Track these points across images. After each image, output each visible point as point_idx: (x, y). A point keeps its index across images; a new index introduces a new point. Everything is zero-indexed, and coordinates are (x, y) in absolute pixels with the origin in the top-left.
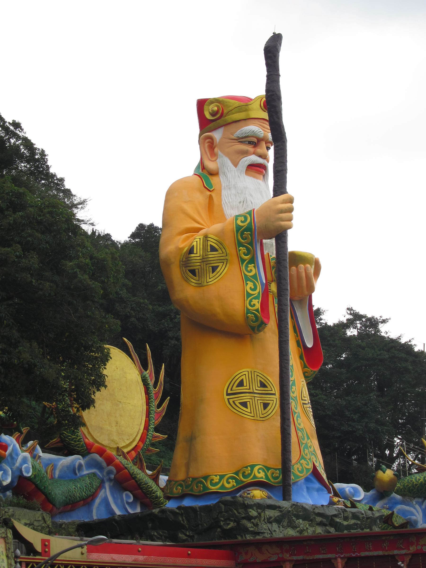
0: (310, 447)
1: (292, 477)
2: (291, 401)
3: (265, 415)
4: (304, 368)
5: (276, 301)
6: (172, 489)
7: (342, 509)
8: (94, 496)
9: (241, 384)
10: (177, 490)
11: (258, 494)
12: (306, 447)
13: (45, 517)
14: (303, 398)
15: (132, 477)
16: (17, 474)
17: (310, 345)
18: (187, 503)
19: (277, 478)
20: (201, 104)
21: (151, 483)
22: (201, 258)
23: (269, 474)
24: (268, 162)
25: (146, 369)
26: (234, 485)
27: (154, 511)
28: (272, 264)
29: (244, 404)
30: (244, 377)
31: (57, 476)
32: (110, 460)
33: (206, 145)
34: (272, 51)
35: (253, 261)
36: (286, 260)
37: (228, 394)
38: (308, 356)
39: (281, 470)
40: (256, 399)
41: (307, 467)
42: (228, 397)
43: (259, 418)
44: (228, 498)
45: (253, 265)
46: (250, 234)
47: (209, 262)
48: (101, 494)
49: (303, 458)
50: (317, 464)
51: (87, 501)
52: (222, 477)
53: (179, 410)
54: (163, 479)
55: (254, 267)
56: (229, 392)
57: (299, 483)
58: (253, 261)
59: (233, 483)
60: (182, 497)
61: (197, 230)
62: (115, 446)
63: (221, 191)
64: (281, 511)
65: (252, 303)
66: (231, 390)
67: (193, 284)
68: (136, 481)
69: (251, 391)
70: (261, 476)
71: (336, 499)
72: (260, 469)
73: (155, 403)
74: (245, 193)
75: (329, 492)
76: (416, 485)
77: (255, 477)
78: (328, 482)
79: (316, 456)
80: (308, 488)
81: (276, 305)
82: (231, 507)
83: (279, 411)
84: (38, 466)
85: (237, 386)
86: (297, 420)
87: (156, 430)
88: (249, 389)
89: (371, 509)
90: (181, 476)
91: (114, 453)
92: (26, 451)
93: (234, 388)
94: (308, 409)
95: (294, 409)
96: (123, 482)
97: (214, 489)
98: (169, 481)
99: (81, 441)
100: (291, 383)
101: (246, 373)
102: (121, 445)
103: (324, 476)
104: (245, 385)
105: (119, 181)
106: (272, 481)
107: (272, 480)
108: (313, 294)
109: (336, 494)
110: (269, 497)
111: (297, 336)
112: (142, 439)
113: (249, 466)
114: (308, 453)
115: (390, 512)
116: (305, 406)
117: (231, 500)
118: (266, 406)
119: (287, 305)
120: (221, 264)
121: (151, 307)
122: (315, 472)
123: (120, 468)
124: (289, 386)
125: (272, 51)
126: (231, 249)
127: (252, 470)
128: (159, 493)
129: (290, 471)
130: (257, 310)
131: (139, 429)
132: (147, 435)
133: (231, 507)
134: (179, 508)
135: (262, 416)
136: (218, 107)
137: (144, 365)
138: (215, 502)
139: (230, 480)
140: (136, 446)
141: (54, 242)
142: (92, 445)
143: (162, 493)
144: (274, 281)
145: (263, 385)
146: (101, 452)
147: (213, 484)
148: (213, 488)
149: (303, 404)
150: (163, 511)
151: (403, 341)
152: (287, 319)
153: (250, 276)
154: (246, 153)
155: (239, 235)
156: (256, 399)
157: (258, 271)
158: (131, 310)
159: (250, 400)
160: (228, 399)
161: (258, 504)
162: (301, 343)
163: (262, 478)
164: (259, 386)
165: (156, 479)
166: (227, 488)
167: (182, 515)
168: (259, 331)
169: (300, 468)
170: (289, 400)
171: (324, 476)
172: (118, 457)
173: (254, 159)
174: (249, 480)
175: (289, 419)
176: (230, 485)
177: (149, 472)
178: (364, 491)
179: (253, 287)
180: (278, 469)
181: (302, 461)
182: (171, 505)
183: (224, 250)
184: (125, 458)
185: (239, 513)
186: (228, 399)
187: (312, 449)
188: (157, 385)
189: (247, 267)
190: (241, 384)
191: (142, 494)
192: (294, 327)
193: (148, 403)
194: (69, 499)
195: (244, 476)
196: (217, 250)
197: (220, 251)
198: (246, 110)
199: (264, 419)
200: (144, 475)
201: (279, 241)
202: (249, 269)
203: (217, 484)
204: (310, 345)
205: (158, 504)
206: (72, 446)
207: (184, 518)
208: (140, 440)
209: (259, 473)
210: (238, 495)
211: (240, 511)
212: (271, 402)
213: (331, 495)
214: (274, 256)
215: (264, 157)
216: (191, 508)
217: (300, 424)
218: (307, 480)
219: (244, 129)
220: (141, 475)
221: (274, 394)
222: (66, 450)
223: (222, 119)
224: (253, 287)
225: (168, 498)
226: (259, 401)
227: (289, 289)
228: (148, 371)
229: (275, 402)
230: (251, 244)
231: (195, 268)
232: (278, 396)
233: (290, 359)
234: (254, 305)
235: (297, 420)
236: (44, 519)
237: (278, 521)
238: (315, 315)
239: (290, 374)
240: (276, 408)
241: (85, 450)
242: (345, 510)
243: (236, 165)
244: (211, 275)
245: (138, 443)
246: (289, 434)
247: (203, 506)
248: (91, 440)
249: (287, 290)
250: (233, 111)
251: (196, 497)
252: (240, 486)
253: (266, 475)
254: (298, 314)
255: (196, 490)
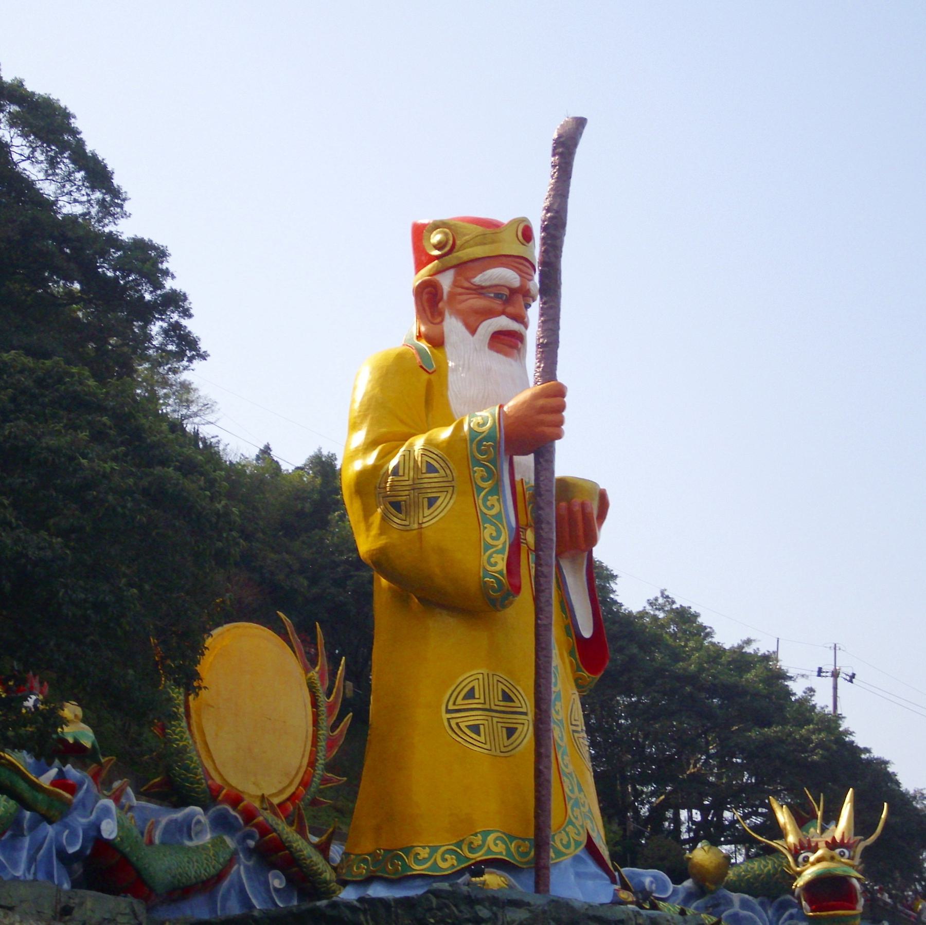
0: (584, 806)
1: (552, 854)
2: (553, 725)
3: (510, 748)
4: (578, 671)
5: (532, 557)
6: (350, 867)
7: (633, 911)
8: (220, 876)
9: (470, 694)
10: (362, 870)
11: (493, 880)
12: (577, 804)
13: (136, 909)
14: (574, 723)
15: (280, 845)
16: (93, 833)
17: (587, 633)
18: (377, 891)
19: (526, 854)
20: (419, 233)
21: (317, 858)
22: (410, 482)
23: (513, 847)
24: (526, 326)
25: (314, 663)
26: (453, 865)
27: (318, 903)
28: (527, 496)
29: (475, 729)
30: (475, 683)
31: (157, 840)
32: (249, 815)
33: (425, 297)
34: (565, 147)
35: (496, 489)
36: (551, 491)
37: (448, 711)
39: (533, 843)
40: (495, 720)
41: (576, 837)
42: (449, 716)
43: (498, 753)
44: (445, 886)
45: (496, 497)
46: (493, 447)
47: (423, 491)
49: (571, 823)
50: (594, 835)
52: (434, 849)
53: (367, 735)
54: (336, 851)
55: (498, 500)
56: (451, 707)
57: (562, 866)
58: (496, 489)
59: (452, 860)
60: (369, 880)
62: (260, 793)
63: (446, 376)
64: (530, 911)
65: (492, 560)
66: (454, 704)
67: (395, 526)
68: (291, 852)
69: (487, 706)
70: (498, 849)
71: (624, 895)
72: (497, 839)
73: (325, 722)
74: (483, 391)
75: (614, 881)
76: (759, 875)
77: (489, 851)
78: (613, 865)
79: (592, 820)
80: (578, 875)
81: (533, 565)
82: (446, 901)
83: (533, 743)
84: (127, 824)
85: (465, 698)
86: (563, 759)
87: (329, 767)
88: (485, 703)
89: (683, 913)
90: (367, 845)
91: (257, 804)
92: (109, 797)
93: (459, 701)
94: (581, 740)
95: (569, 793)
96: (271, 853)
97: (418, 869)
98: (346, 854)
99: (202, 784)
100: (553, 697)
101: (480, 676)
102: (267, 793)
103: (605, 852)
104: (477, 696)
105: (281, 369)
106: (516, 860)
107: (517, 857)
108: (594, 549)
109: (625, 887)
110: (511, 887)
111: (567, 618)
112: (305, 784)
113: (479, 833)
114: (580, 811)
115: (715, 919)
116: (576, 735)
117: (450, 889)
118: (511, 732)
119: (552, 549)
120: (443, 495)
122: (591, 847)
123: (265, 830)
124: (550, 700)
125: (565, 147)
127: (484, 841)
128: (329, 875)
129: (548, 844)
130: (500, 573)
131: (300, 767)
132: (314, 776)
133: (446, 901)
134: (361, 900)
135: (503, 749)
136: (446, 234)
137: (310, 661)
138: (420, 892)
139: (447, 856)
140: (294, 794)
142: (221, 788)
143: (334, 875)
144: (531, 526)
145: (507, 697)
146: (235, 800)
147: (418, 861)
148: (417, 867)
149: (574, 731)
150: (335, 905)
151: (891, 769)
152: (550, 589)
153: (492, 516)
154: (489, 313)
155: (474, 446)
156: (495, 720)
157: (503, 507)
159: (485, 722)
160: (448, 719)
161: (494, 897)
163: (501, 853)
164: (501, 698)
165: (323, 849)
166: (442, 869)
167: (365, 912)
168: (504, 607)
169: (565, 842)
170: (549, 725)
171: (605, 852)
172: (261, 811)
173: (504, 322)
174: (479, 856)
175: (549, 756)
176: (447, 865)
177: (315, 840)
178: (673, 883)
179: (494, 534)
180: (528, 840)
181: (570, 828)
182: (348, 894)
183: (448, 472)
184: (275, 814)
185: (461, 912)
186: (448, 719)
187: (586, 809)
188: (337, 727)
189: (485, 499)
190: (470, 694)
191: (302, 880)
192: (558, 582)
193: (316, 723)
194: (179, 880)
195: (472, 849)
196: (437, 471)
197: (442, 471)
198: (493, 242)
199: (506, 754)
200: (304, 846)
201: (541, 460)
202: (489, 503)
203: (425, 860)
204: (587, 633)
205: (329, 893)
206: (196, 793)
207: (369, 917)
208: (300, 784)
209: (496, 845)
210: (459, 881)
211: (462, 908)
212: (520, 727)
213: (617, 887)
214: (532, 483)
215: (521, 319)
216: (381, 900)
217: (566, 766)
219: (491, 281)
220: (300, 843)
221: (525, 714)
223: (455, 255)
224: (494, 534)
225: (344, 883)
226: (500, 725)
227: (555, 539)
228: (317, 668)
229: (526, 728)
230: (494, 462)
231: (400, 498)
232: (531, 716)
233: (554, 655)
234: (496, 564)
235: (563, 759)
236: (134, 912)
238: (598, 580)
239: (553, 680)
240: (525, 741)
241: (210, 797)
242: (638, 912)
243: (473, 331)
244: (427, 512)
245: (297, 789)
246: (549, 781)
247: (401, 898)
248: (218, 781)
249: (552, 540)
250: (471, 242)
251: (390, 882)
252: (463, 866)
253: (508, 849)
254: (570, 580)
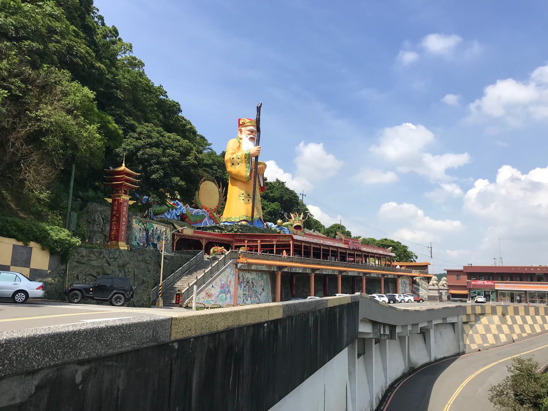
8: (203, 220)
18: (226, 224)
34: (259, 109)
38: (262, 189)
48: (205, 220)
51: (201, 222)
61: (235, 153)
121: (194, 148)
125: (259, 109)
126: (244, 160)
141: (481, 299)
146: (206, 209)
158: (79, 16)
162: (260, 185)
176: (238, 220)
218: (258, 220)
222: (196, 207)
237: (249, 230)
255: (228, 221)
